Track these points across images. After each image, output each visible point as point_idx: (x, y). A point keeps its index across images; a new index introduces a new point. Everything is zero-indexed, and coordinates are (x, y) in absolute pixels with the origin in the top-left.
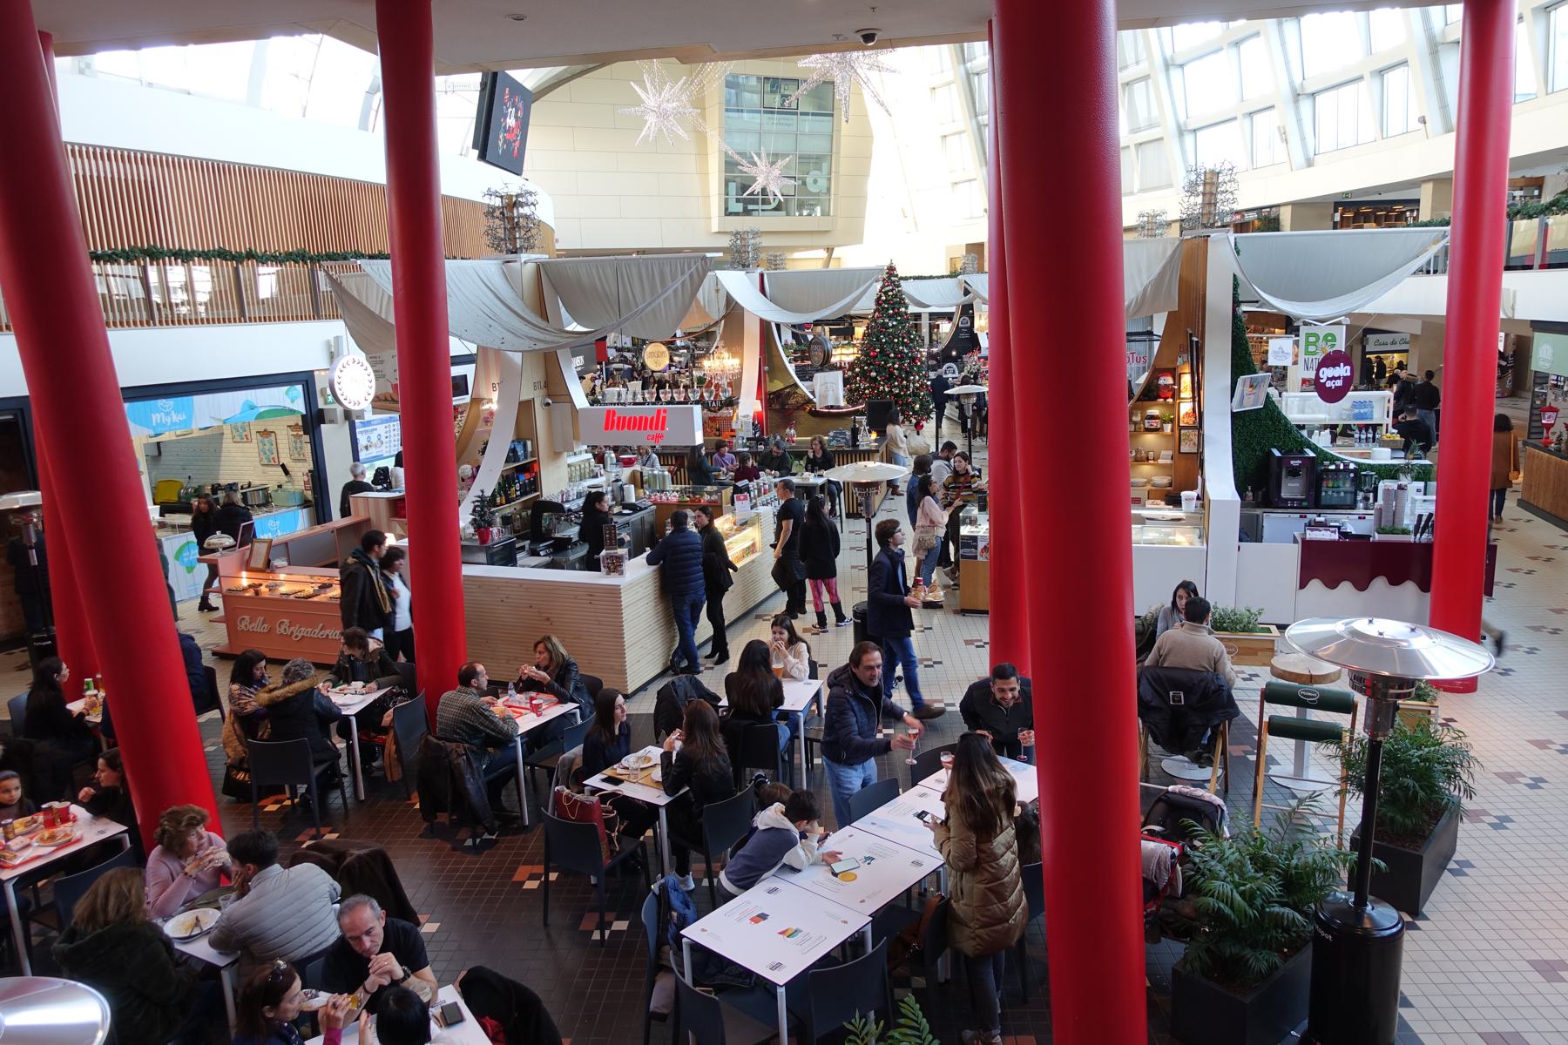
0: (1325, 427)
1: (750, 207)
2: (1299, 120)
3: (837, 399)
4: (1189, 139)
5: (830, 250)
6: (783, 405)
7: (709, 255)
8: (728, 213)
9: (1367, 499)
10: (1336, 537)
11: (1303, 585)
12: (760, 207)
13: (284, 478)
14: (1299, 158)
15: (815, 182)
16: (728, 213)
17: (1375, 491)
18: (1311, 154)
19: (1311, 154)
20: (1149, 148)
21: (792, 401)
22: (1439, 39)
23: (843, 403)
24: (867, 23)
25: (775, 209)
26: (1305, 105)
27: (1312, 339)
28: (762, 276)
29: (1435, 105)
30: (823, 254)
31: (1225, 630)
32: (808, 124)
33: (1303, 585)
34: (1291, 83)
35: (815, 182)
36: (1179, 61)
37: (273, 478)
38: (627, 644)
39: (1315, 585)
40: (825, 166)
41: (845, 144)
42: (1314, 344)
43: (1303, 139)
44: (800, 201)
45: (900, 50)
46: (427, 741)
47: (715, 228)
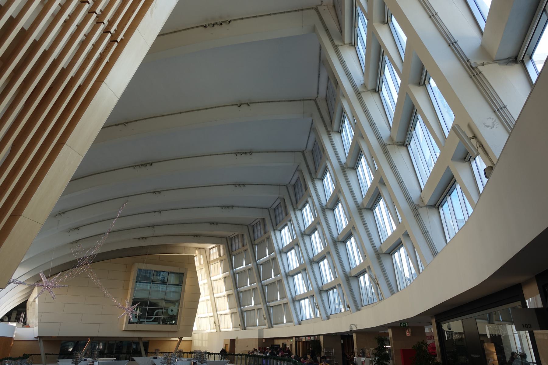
1: (141, 320)
2: (322, 301)
5: (181, 339)
8: (130, 322)
12: (146, 320)
14: (324, 316)
16: (130, 322)
18: (329, 314)
19: (329, 314)
22: (349, 275)
25: (153, 321)
26: (324, 295)
29: (352, 301)
30: (177, 339)
32: (173, 289)
34: (318, 286)
35: (172, 311)
36: (291, 274)
38: (201, 299)
40: (177, 304)
41: (186, 297)
43: (325, 308)
45: (340, 65)
46: (287, 322)
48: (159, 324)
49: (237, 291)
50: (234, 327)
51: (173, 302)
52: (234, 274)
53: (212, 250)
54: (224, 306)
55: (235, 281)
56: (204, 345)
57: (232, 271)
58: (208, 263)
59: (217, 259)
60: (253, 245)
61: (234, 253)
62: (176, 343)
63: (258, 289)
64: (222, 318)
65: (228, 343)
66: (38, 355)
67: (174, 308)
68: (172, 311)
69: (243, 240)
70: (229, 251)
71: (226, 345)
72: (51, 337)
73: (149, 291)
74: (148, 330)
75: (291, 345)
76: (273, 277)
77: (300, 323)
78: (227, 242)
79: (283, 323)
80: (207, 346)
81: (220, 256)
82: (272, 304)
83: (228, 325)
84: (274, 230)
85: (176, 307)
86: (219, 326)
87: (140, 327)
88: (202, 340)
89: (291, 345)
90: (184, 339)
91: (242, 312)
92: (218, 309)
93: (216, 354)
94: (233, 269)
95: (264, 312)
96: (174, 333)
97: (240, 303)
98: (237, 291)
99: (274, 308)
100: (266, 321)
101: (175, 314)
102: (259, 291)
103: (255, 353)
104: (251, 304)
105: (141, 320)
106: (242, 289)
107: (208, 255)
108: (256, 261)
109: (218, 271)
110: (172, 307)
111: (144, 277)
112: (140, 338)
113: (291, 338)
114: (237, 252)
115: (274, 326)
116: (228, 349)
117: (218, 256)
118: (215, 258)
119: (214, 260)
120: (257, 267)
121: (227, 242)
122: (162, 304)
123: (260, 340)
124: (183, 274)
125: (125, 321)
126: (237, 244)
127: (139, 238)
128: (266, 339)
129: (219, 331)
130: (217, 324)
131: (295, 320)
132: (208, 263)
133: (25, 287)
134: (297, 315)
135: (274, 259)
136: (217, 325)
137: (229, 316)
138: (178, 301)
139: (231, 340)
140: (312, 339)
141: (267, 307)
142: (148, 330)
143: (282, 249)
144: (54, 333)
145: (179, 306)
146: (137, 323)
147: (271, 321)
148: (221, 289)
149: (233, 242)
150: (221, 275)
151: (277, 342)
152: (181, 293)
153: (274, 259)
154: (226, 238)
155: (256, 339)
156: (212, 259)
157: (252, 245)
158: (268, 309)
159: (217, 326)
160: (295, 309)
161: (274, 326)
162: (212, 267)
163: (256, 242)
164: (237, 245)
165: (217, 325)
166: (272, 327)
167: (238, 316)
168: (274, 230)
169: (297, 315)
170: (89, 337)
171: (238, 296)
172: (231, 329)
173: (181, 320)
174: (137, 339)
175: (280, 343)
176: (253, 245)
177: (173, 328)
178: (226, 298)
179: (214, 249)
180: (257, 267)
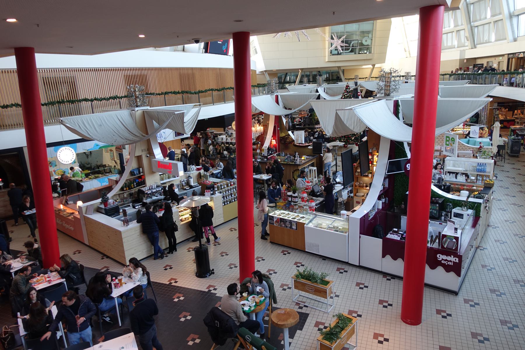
0: (463, 174)
3: (302, 141)
4: (515, 20)
5: (374, 65)
6: (285, 141)
7: (176, 113)
9: (447, 215)
10: (399, 239)
11: (384, 256)
13: (115, 164)
15: (366, 41)
17: (451, 212)
20: (500, 22)
21: (288, 140)
23: (304, 143)
24: (196, 37)
27: (448, 139)
28: (277, 97)
30: (371, 66)
31: (310, 280)
33: (384, 256)
35: (366, 41)
37: (112, 164)
39: (388, 257)
42: (448, 141)
44: (363, 48)
46: (496, 41)
47: (327, 60)
48: (355, 54)
62: (370, 71)
72: (272, 70)
74: (347, 59)
77: (515, 40)
82: (476, 24)
87: (339, 58)
90: (376, 66)
93: (121, 97)
96: (367, 61)
101: (369, 44)
103: (459, 72)
113: (503, 55)
115: (478, 46)
123: (461, 61)
125: (327, 53)
128: (468, 59)
129: (408, 56)
130: (407, 50)
131: (511, 37)
134: (513, 32)
140: (138, 73)
144: (275, 67)
155: (456, 60)
158: (472, 29)
159: (408, 52)
160: (512, 25)
161: (478, 46)
166: (475, 47)
169: (513, 32)
170: (299, 69)
173: (375, 49)
175: (484, 62)
177: (368, 56)
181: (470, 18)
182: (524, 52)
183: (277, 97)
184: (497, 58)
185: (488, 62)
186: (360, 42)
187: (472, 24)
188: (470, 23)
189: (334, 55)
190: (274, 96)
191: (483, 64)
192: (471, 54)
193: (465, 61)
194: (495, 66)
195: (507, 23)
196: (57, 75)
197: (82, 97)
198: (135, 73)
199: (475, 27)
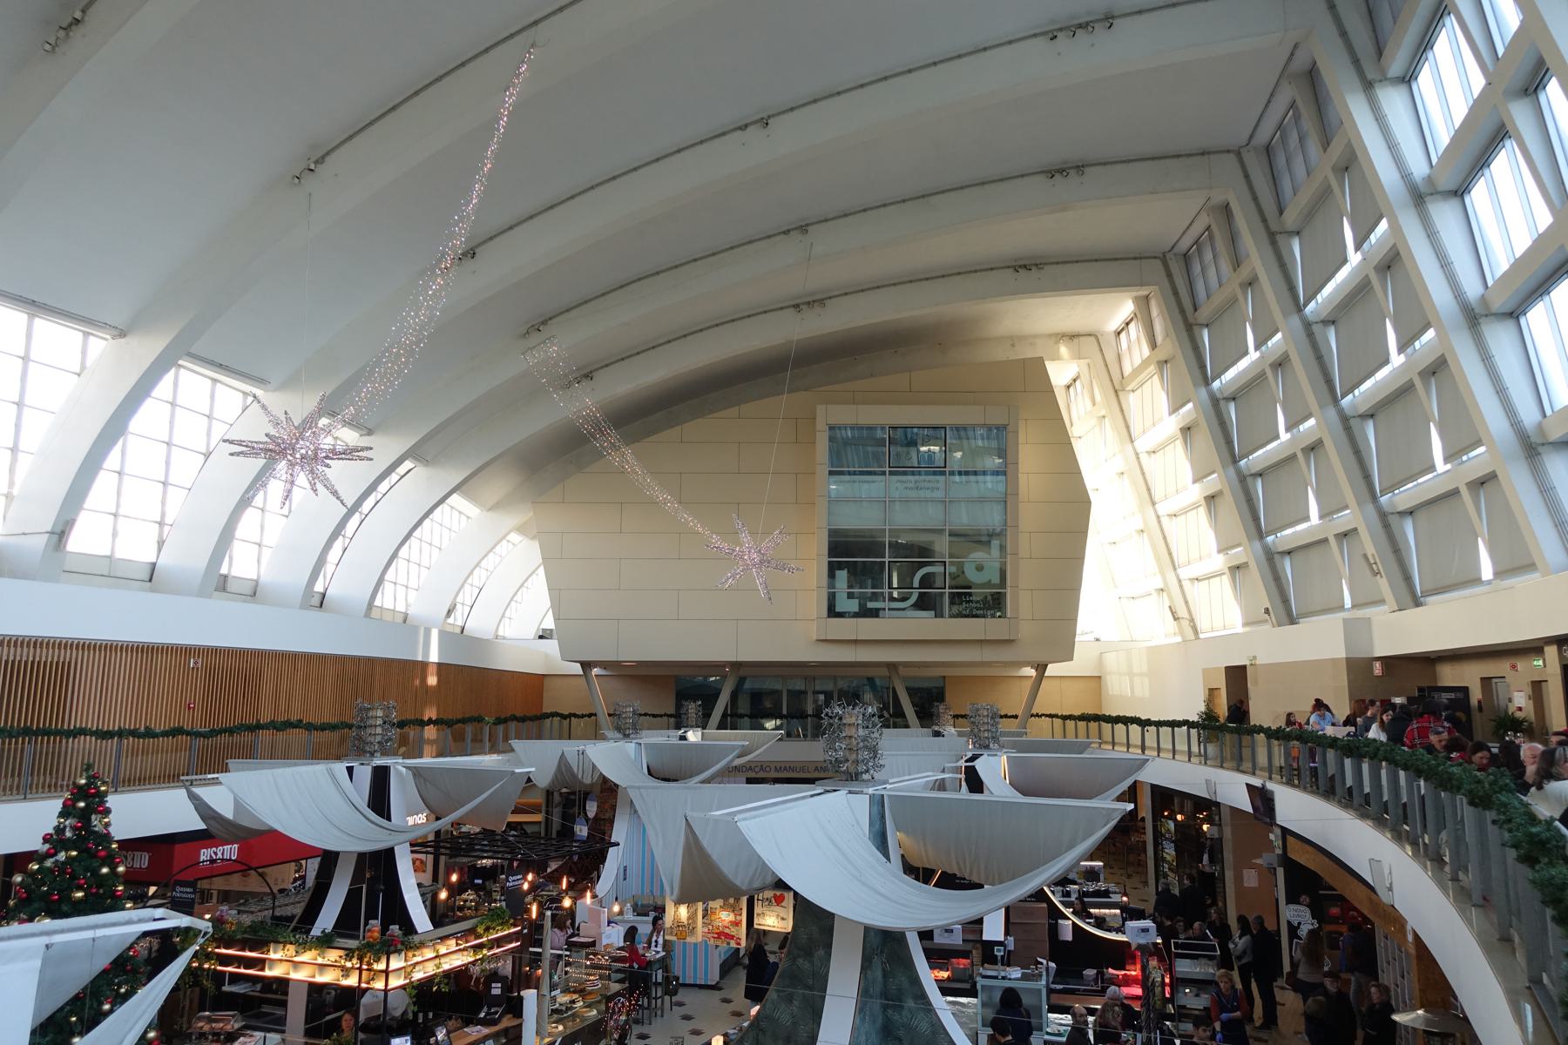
5: (1041, 668)
8: (833, 613)
28: (381, 778)
40: (995, 543)
46: (1499, 574)
49: (1239, 473)
50: (1245, 625)
51: (982, 539)
52: (1216, 404)
53: (1123, 335)
54: (1201, 543)
55: (1223, 430)
56: (1138, 693)
57: (1203, 392)
58: (1117, 389)
59: (1145, 363)
60: (1274, 239)
61: (1204, 313)
62: (1028, 685)
63: (1328, 443)
64: (1196, 593)
65: (1221, 683)
66: (590, 715)
67: (989, 558)
68: (980, 568)
69: (1233, 239)
70: (1182, 311)
71: (1212, 692)
73: (880, 505)
74: (903, 635)
75: (1537, 687)
76: (1441, 467)
78: (1169, 275)
79: (1477, 581)
80: (1147, 694)
81: (1153, 345)
83: (1224, 614)
84: (1368, 86)
85: (995, 552)
86: (1192, 620)
88: (1131, 675)
89: (1537, 687)
90: (1052, 670)
91: (1271, 558)
92: (1180, 558)
94: (1207, 382)
95: (1368, 544)
97: (1256, 519)
98: (1239, 473)
99: (1422, 516)
100: (1383, 584)
102: (1334, 454)
104: (1307, 518)
105: (870, 605)
106: (1260, 457)
107: (1110, 357)
108: (1299, 309)
109: (1157, 412)
110: (978, 555)
111: (861, 452)
112: (892, 666)
113: (1533, 648)
114: (1217, 300)
116: (1222, 710)
117: (1146, 351)
118: (1138, 361)
119: (1137, 371)
120: (1310, 335)
121: (1169, 275)
122: (942, 546)
123: (1358, 667)
124: (1005, 427)
126: (1212, 273)
127: (796, 306)
128: (1388, 661)
129: (1190, 635)
130: (1182, 612)
132: (1117, 389)
133: (1532, 717)
135: (1438, 369)
136: (1185, 618)
137: (1226, 579)
138: (1000, 534)
139: (1227, 669)
141: (1383, 516)
142: (903, 635)
143: (1429, 180)
145: (1002, 548)
146: (856, 615)
147: (1408, 579)
148: (1179, 478)
149: (1197, 269)
150: (1171, 425)
151: (1449, 676)
152: (1006, 501)
153: (1438, 369)
154: (1163, 258)
156: (1128, 370)
157: (1272, 237)
159: (1185, 623)
162: (1132, 401)
163: (1291, 218)
164: (1214, 275)
165: (1185, 618)
167: (1255, 576)
168: (1368, 86)
171: (1248, 498)
172: (1240, 629)
173: (1022, 600)
174: (884, 672)
175: (1468, 676)
176: (1274, 239)
178: (1202, 511)
179: (1132, 326)
180: (1310, 335)
181: (1367, 478)
182: (1564, 641)
183: (381, 778)
184: (1521, 664)
185: (1486, 682)
186: (951, 569)
187: (1384, 500)
188: (1374, 498)
189: (840, 615)
190: (364, 774)
191: (1465, 690)
192: (1406, 632)
193: (1377, 669)
194: (1520, 701)
195: (1518, 483)
196: (43, 655)
197: (75, 722)
198: (26, 654)
199: (1403, 514)
